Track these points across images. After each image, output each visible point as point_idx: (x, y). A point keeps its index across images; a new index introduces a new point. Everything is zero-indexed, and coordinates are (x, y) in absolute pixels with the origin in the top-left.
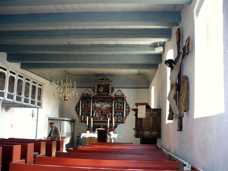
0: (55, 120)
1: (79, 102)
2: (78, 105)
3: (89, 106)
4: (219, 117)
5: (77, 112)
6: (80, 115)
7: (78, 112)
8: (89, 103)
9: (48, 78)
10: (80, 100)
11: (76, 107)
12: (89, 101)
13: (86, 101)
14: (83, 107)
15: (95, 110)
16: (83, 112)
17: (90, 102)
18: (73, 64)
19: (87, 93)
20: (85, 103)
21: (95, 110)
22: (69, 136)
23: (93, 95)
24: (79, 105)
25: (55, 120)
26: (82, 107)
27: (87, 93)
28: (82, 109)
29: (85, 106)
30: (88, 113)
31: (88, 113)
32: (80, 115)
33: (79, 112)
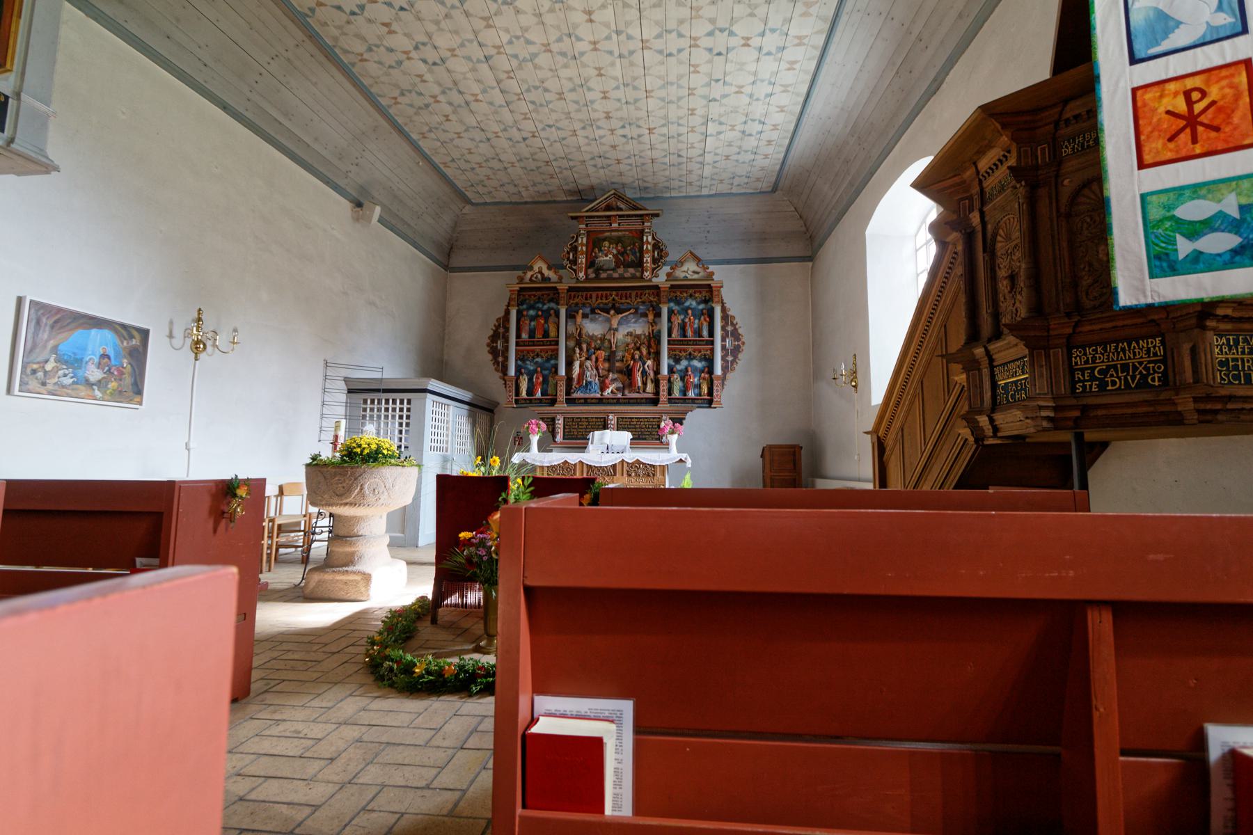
0: (378, 391)
2: (501, 330)
3: (552, 334)
5: (496, 362)
7: (500, 359)
8: (552, 319)
10: (509, 305)
11: (494, 337)
13: (539, 309)
14: (525, 336)
15: (581, 349)
17: (557, 315)
20: (533, 319)
24: (507, 330)
25: (378, 391)
26: (518, 336)
27: (542, 274)
30: (547, 365)
33: (506, 359)
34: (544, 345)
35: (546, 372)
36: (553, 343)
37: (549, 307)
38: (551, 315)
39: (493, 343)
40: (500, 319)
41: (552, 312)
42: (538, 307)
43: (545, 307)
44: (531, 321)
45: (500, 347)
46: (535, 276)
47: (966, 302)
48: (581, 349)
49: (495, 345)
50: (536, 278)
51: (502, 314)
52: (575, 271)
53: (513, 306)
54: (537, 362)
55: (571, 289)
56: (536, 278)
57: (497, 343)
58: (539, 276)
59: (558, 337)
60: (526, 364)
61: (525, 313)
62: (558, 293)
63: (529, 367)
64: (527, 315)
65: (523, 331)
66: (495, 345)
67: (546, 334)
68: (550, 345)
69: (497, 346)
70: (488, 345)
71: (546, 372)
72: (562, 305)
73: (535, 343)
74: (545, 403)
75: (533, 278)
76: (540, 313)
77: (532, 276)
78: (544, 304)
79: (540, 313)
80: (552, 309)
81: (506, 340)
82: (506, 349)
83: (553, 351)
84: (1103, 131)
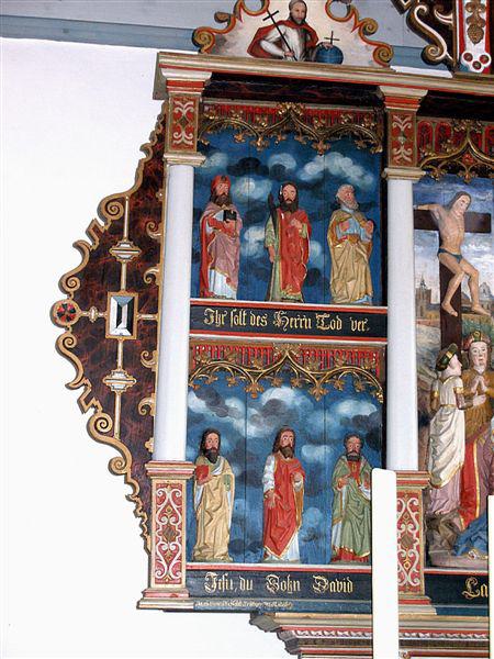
1: (152, 177)
2: (125, 252)
3: (351, 289)
4: (230, 161)
5: (96, 393)
6: (171, 443)
8: (351, 225)
9: (380, 212)
12: (329, 181)
13: (279, 176)
14: (222, 285)
15: (467, 364)
16: (215, 399)
17: (375, 206)
18: (472, 452)
19: (298, 23)
20: (255, 214)
21: (455, 367)
22: (227, 408)
23: (409, 80)
24: (151, 252)
26: (200, 285)
27: (307, 33)
28: (197, 318)
29: (253, 274)
30: (321, 421)
31: (321, 421)
32: (171, 443)
33: (147, 381)
34: (315, 332)
35: (317, 454)
36: (358, 325)
37: (326, 173)
38: (336, 206)
39: (85, 306)
40: (120, 199)
41: (343, 193)
42: (279, 168)
43: (312, 170)
44: (248, 223)
45: (117, 331)
46: (274, 34)
47: (255, 179)
48: (467, 364)
49: (93, 314)
50: (280, 43)
51: (124, 180)
52: (447, 31)
53: (180, 147)
54: (274, 403)
55: (436, 103)
56: (280, 43)
57: (103, 307)
58: (293, 38)
59: (385, 302)
60: (226, 411)
61: (221, 188)
62: (385, 119)
63: (239, 424)
64: (228, 199)
65: (220, 262)
66: (93, 314)
67: (316, 281)
68: (346, 332)
69: (102, 322)
70: (61, 314)
71: (317, 454)
72: (403, 163)
73: (279, 322)
74: (281, 595)
75: (268, 46)
76: (289, 192)
77: (262, 33)
78: (305, 155)
79: (289, 192)
80: (341, 180)
81: (149, 297)
82: (149, 336)
83: (357, 356)
84: (420, 358)
